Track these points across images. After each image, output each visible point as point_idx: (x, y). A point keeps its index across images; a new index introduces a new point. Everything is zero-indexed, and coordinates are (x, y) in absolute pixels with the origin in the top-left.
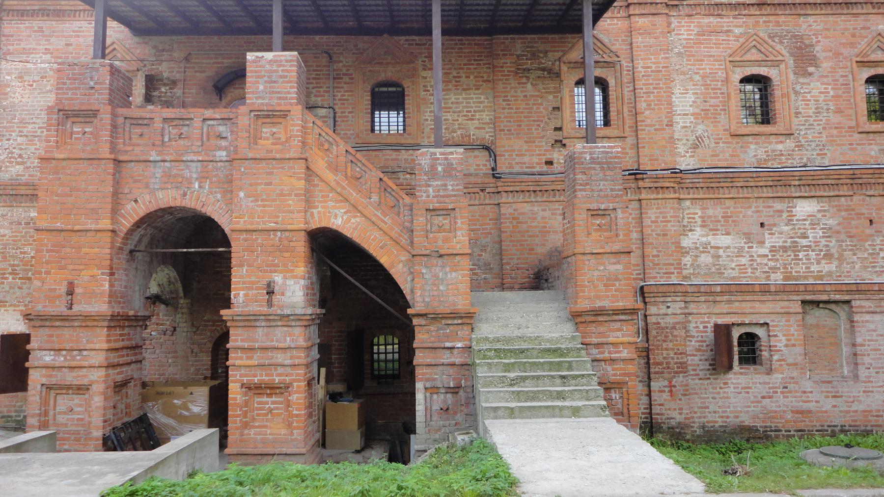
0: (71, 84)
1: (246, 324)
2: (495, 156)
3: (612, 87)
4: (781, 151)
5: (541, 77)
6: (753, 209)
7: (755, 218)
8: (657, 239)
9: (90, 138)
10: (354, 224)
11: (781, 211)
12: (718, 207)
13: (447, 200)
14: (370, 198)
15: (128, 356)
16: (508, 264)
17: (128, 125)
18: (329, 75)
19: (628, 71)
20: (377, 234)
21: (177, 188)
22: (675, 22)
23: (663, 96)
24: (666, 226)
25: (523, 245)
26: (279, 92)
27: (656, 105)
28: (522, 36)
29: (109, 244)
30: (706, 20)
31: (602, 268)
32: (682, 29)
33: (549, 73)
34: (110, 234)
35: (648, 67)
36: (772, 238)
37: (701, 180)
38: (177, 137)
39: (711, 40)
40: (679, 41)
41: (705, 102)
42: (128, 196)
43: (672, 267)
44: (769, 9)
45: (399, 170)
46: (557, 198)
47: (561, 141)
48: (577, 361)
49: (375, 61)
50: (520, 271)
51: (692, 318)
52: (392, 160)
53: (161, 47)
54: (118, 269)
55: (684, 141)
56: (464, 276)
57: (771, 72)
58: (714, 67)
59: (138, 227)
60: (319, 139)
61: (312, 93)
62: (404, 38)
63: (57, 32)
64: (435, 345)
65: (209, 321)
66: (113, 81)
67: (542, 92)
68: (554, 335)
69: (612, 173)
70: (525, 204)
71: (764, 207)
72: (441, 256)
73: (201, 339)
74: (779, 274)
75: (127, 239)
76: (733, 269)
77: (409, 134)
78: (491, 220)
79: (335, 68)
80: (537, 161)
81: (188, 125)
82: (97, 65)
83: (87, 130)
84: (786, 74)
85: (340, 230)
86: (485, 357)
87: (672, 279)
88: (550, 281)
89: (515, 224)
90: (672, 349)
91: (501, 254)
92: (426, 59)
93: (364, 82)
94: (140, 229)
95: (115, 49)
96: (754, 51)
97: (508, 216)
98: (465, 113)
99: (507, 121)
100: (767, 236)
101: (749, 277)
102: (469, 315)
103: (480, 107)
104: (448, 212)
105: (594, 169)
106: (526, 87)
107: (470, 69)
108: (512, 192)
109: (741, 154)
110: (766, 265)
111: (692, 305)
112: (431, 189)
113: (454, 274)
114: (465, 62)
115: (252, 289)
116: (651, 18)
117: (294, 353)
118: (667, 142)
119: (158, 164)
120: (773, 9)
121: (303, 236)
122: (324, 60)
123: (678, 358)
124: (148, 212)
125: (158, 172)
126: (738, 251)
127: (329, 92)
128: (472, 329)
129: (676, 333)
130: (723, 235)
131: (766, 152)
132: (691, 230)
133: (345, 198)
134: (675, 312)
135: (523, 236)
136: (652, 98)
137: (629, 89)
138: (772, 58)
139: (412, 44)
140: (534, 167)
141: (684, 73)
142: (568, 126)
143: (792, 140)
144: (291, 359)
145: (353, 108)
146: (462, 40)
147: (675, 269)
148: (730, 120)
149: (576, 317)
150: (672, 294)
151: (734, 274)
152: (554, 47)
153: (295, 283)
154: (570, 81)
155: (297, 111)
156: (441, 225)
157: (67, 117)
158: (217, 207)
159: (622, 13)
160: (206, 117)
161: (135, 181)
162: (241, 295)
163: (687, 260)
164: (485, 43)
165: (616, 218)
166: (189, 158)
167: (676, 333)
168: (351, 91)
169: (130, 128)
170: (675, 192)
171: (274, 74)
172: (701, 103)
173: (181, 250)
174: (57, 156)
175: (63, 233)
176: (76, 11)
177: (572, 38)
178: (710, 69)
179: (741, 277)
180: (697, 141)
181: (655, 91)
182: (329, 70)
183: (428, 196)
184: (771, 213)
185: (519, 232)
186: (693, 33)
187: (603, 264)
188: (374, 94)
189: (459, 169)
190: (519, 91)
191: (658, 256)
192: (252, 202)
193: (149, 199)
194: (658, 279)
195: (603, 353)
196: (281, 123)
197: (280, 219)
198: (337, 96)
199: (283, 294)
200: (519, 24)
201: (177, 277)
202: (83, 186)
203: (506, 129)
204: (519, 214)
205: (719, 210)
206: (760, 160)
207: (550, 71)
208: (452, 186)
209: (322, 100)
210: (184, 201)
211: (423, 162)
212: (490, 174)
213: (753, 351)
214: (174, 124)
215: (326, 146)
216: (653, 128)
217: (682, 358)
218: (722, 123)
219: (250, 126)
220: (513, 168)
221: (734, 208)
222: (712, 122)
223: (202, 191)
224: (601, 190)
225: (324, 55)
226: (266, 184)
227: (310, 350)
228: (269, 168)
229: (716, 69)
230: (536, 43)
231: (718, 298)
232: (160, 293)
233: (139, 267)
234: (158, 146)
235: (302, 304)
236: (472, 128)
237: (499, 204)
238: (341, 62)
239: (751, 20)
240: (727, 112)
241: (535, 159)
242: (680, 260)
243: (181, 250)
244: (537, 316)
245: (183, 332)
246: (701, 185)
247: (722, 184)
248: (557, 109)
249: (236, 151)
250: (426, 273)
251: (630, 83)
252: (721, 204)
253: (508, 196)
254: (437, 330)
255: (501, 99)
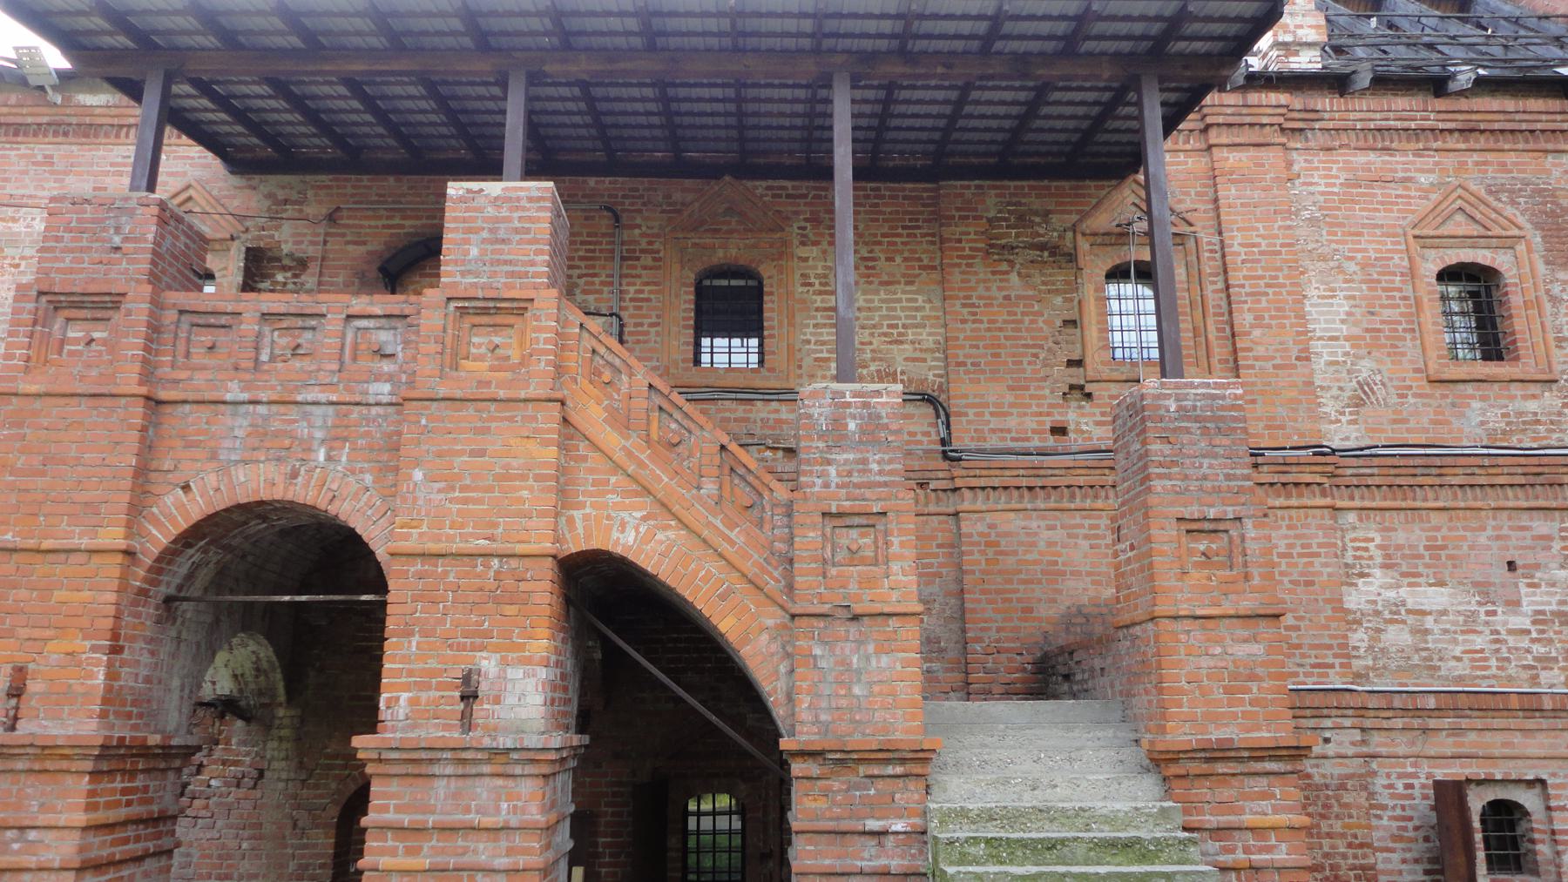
0: (73, 240)
1: (411, 769)
2: (947, 416)
3: (1181, 282)
4: (1535, 414)
5: (1038, 262)
6: (1489, 532)
7: (1495, 551)
8: (1290, 591)
9: (100, 352)
10: (661, 542)
11: (1549, 538)
12: (1416, 527)
13: (868, 493)
14: (699, 488)
15: (138, 839)
16: (978, 640)
17: (185, 326)
18: (612, 251)
19: (1211, 251)
20: (713, 567)
21: (279, 459)
22: (1299, 162)
23: (1286, 302)
24: (1311, 564)
25: (1010, 600)
26: (510, 262)
27: (1272, 317)
28: (998, 183)
29: (116, 582)
30: (1361, 159)
31: (1218, 650)
32: (1315, 173)
33: (1052, 254)
34: (119, 558)
35: (1254, 245)
36: (1534, 594)
37: (1376, 471)
38: (289, 352)
39: (1375, 195)
40: (1311, 197)
41: (1372, 314)
42: (170, 476)
43: (1329, 653)
44: (1482, 138)
45: (750, 441)
46: (1078, 503)
47: (1081, 388)
48: (1186, 873)
49: (706, 227)
50: (1003, 656)
51: (1380, 765)
52: (736, 420)
53: (281, 195)
54: (133, 639)
55: (1335, 392)
56: (906, 663)
57: (1500, 260)
58: (1384, 248)
59: (189, 545)
60: (592, 360)
61: (577, 285)
62: (764, 184)
63: (80, 164)
64: (845, 825)
65: (336, 757)
66: (163, 237)
67: (1040, 291)
68: (1118, 806)
69: (1225, 441)
70: (1012, 515)
71: (1511, 528)
72: (856, 618)
73: (316, 797)
74: (1556, 671)
75: (160, 571)
76: (1459, 659)
77: (771, 370)
78: (939, 546)
79: (626, 238)
80: (1035, 426)
81: (313, 329)
82: (132, 204)
83: (96, 335)
84: (1530, 263)
85: (631, 557)
86: (963, 859)
87: (1332, 678)
88: (1079, 677)
89: (990, 556)
90: (1343, 836)
91: (963, 619)
92: (808, 224)
93: (683, 268)
94: (191, 551)
95: (190, 198)
96: (1459, 217)
97: (976, 538)
98: (885, 329)
99: (972, 346)
100: (1524, 590)
101: (1494, 676)
102: (921, 755)
103: (915, 317)
104: (871, 520)
105: (1187, 431)
106: (1007, 281)
107: (895, 244)
108: (983, 488)
109: (1453, 420)
110: (1528, 651)
111: (1376, 738)
112: (832, 470)
113: (885, 660)
114: (886, 230)
115: (425, 686)
116: (1252, 152)
117: (518, 840)
118: (1300, 393)
119: (243, 409)
120: (1492, 139)
121: (547, 569)
122: (605, 222)
123: (1355, 857)
124: (212, 511)
125: (240, 424)
126: (1465, 621)
127: (611, 284)
128: (928, 786)
129: (1347, 798)
130: (1431, 585)
131: (1504, 415)
132: (1362, 575)
133: (644, 487)
134: (1343, 751)
135: (1010, 581)
136: (1264, 304)
137: (1215, 287)
138: (1497, 231)
139: (780, 196)
140: (1027, 439)
141: (1323, 258)
142: (1096, 356)
143: (1555, 393)
144: (507, 855)
145: (658, 316)
146: (878, 189)
147: (1336, 656)
148: (1424, 350)
149: (1162, 763)
150: (1334, 712)
151: (1462, 669)
152: (1062, 204)
153: (526, 675)
154: (1097, 271)
155: (547, 300)
156: (854, 547)
157: (56, 309)
158: (362, 503)
159: (1194, 143)
160: (355, 310)
161: (190, 445)
162: (402, 702)
163: (1359, 638)
164: (925, 195)
165: (1243, 538)
166: (310, 397)
167: (1347, 798)
168: (655, 284)
169: (190, 333)
170: (1324, 494)
171: (502, 225)
172: (1363, 315)
173: (277, 598)
174: (24, 387)
175: (15, 556)
176: (122, 126)
177: (1097, 187)
178: (1376, 251)
179: (1478, 677)
180: (1360, 392)
181: (1270, 291)
182: (613, 243)
183: (826, 485)
184: (1529, 542)
185: (1000, 572)
186: (1337, 181)
187: (1219, 641)
188: (701, 292)
189: (894, 427)
190: (994, 288)
191: (1297, 628)
192: (440, 491)
193: (215, 484)
194: (1302, 678)
195: (1232, 851)
196: (512, 326)
197: (500, 530)
198: (627, 292)
199: (497, 700)
200: (991, 160)
201: (274, 658)
202: (73, 454)
203: (969, 361)
204: (998, 535)
205: (1418, 532)
206: (1491, 434)
207: (1054, 250)
208: (879, 463)
209: (596, 300)
210: (291, 488)
211: (816, 412)
212: (936, 451)
213: (1514, 843)
214: (285, 325)
215: (607, 375)
216: (1270, 364)
217: (1365, 856)
218: (1409, 357)
219: (445, 331)
220: (985, 440)
221: (1450, 529)
222: (1389, 355)
223: (332, 467)
224: (1205, 478)
225: (605, 213)
226: (473, 453)
227: (553, 833)
228: (481, 419)
229: (1389, 251)
230: (1024, 196)
231: (1432, 723)
232: (235, 693)
233: (184, 635)
234: (246, 370)
235: (540, 725)
236: (899, 359)
237: (956, 514)
238: (639, 226)
239: (1450, 160)
240: (1418, 334)
241: (1031, 423)
242: (1345, 637)
243: (277, 598)
244: (1070, 760)
245: (279, 779)
246: (1377, 480)
247: (1420, 480)
248: (1073, 323)
249: (411, 383)
250: (822, 657)
251: (1217, 275)
252: (1421, 520)
253: (975, 498)
254: (848, 790)
255: (958, 303)
